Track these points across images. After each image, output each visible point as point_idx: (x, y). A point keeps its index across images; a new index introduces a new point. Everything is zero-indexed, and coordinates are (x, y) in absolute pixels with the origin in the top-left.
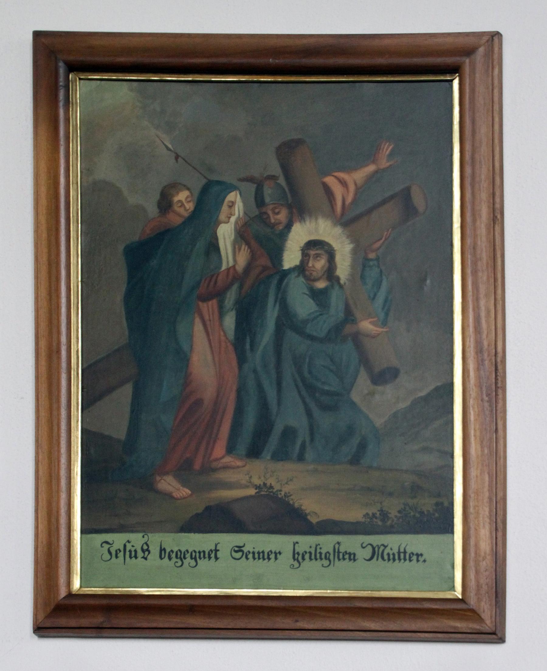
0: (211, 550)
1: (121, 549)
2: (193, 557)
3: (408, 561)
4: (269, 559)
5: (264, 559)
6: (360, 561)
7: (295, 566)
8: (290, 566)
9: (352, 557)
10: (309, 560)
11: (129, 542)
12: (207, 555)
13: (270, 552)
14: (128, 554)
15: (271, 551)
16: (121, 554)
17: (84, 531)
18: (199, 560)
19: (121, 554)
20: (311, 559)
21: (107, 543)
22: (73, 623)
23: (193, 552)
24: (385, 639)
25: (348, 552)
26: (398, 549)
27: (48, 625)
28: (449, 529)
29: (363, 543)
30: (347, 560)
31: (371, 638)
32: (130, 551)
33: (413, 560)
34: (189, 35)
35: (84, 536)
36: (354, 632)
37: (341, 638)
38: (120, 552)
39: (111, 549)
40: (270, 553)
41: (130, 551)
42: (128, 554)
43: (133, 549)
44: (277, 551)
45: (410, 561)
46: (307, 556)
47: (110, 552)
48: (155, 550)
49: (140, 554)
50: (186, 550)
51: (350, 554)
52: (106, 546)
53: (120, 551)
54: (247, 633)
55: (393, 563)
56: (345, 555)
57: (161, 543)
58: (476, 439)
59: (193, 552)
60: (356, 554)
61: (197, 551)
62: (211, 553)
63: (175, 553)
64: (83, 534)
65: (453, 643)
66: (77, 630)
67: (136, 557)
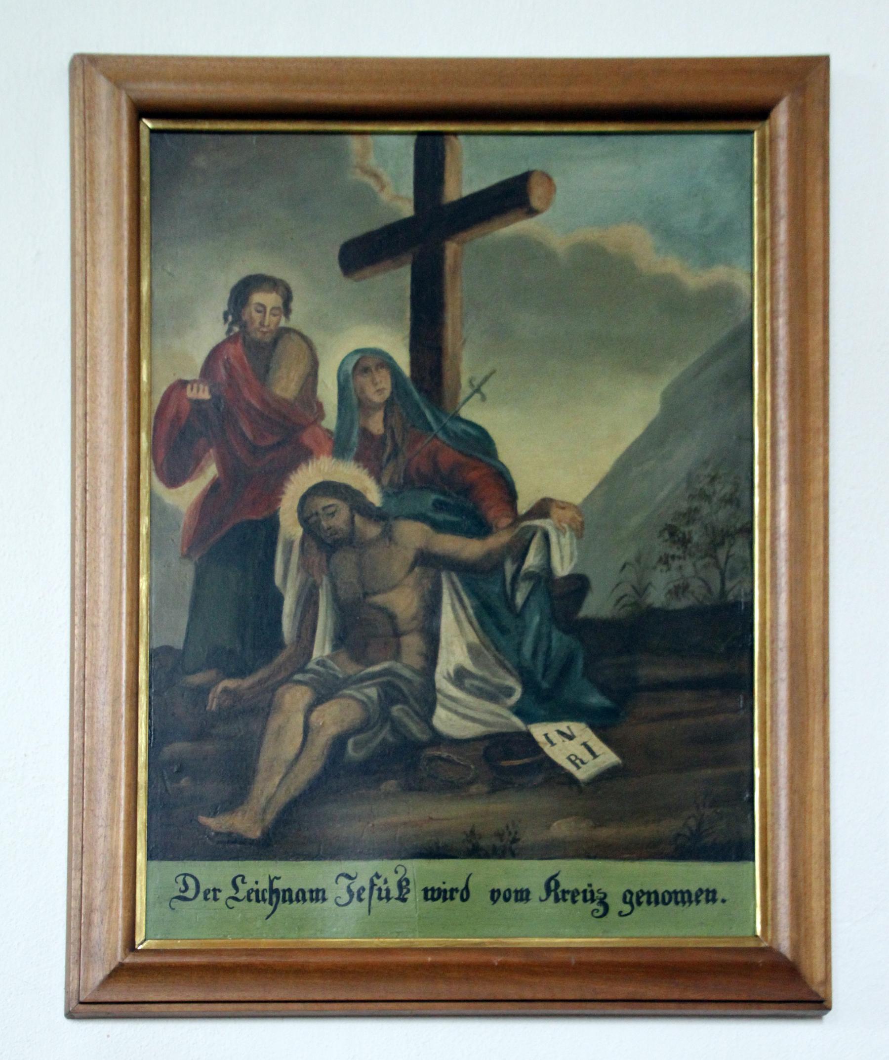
0: (363, 889)
1: (365, 887)
2: (628, 900)
3: (694, 903)
4: (452, 898)
5: (677, 903)
6: (392, 901)
7: (341, 902)
8: (335, 900)
9: (523, 895)
10: (492, 903)
11: (378, 876)
12: (693, 898)
13: (640, 893)
14: (376, 893)
15: (701, 890)
16: (366, 895)
17: (150, 856)
18: (282, 901)
19: (366, 895)
20: (649, 903)
21: (348, 877)
22: (512, 992)
23: (666, 894)
24: (389, 1013)
25: (496, 889)
26: (464, 881)
27: (107, 998)
28: (753, 860)
29: (340, 897)
30: (644, 904)
31: (202, 1014)
32: (380, 890)
33: (578, 900)
34: (233, 60)
35: (154, 863)
36: (319, 1004)
37: (365, 1013)
38: (363, 892)
39: (352, 887)
40: (640, 895)
41: (380, 890)
42: (376, 893)
43: (384, 887)
44: (217, 888)
45: (698, 902)
46: (580, 898)
47: (349, 890)
48: (538, 891)
49: (395, 893)
50: (698, 889)
51: (649, 894)
52: (344, 882)
53: (578, 893)
54: (660, 1009)
55: (387, 902)
56: (641, 897)
57: (468, 880)
58: (411, 718)
59: (666, 894)
60: (718, 891)
61: (513, 889)
62: (361, 891)
63: (459, 893)
64: (152, 860)
65: (160, 1020)
66: (578, 1004)
67: (304, 900)
